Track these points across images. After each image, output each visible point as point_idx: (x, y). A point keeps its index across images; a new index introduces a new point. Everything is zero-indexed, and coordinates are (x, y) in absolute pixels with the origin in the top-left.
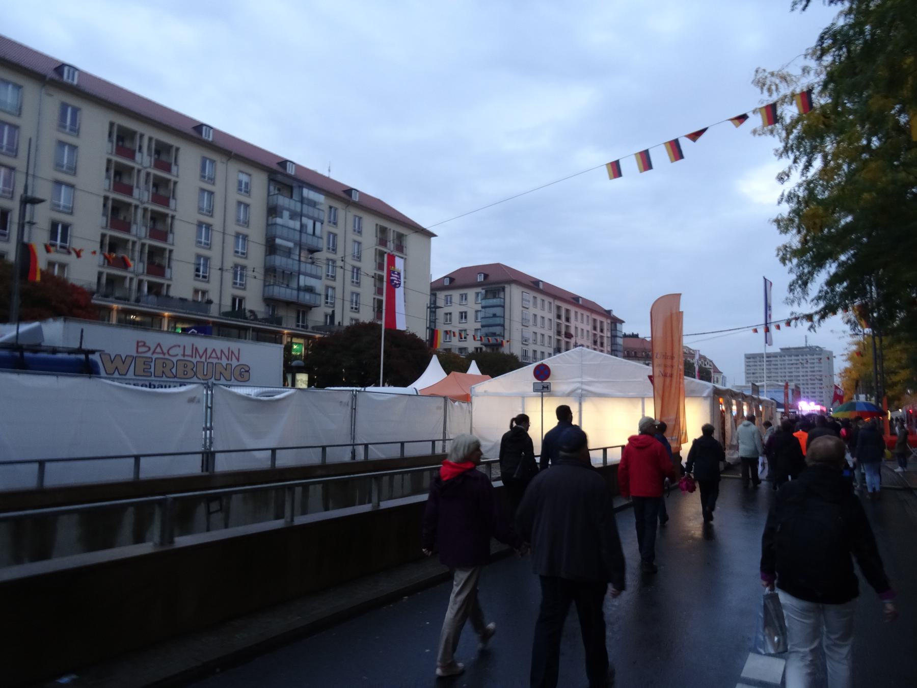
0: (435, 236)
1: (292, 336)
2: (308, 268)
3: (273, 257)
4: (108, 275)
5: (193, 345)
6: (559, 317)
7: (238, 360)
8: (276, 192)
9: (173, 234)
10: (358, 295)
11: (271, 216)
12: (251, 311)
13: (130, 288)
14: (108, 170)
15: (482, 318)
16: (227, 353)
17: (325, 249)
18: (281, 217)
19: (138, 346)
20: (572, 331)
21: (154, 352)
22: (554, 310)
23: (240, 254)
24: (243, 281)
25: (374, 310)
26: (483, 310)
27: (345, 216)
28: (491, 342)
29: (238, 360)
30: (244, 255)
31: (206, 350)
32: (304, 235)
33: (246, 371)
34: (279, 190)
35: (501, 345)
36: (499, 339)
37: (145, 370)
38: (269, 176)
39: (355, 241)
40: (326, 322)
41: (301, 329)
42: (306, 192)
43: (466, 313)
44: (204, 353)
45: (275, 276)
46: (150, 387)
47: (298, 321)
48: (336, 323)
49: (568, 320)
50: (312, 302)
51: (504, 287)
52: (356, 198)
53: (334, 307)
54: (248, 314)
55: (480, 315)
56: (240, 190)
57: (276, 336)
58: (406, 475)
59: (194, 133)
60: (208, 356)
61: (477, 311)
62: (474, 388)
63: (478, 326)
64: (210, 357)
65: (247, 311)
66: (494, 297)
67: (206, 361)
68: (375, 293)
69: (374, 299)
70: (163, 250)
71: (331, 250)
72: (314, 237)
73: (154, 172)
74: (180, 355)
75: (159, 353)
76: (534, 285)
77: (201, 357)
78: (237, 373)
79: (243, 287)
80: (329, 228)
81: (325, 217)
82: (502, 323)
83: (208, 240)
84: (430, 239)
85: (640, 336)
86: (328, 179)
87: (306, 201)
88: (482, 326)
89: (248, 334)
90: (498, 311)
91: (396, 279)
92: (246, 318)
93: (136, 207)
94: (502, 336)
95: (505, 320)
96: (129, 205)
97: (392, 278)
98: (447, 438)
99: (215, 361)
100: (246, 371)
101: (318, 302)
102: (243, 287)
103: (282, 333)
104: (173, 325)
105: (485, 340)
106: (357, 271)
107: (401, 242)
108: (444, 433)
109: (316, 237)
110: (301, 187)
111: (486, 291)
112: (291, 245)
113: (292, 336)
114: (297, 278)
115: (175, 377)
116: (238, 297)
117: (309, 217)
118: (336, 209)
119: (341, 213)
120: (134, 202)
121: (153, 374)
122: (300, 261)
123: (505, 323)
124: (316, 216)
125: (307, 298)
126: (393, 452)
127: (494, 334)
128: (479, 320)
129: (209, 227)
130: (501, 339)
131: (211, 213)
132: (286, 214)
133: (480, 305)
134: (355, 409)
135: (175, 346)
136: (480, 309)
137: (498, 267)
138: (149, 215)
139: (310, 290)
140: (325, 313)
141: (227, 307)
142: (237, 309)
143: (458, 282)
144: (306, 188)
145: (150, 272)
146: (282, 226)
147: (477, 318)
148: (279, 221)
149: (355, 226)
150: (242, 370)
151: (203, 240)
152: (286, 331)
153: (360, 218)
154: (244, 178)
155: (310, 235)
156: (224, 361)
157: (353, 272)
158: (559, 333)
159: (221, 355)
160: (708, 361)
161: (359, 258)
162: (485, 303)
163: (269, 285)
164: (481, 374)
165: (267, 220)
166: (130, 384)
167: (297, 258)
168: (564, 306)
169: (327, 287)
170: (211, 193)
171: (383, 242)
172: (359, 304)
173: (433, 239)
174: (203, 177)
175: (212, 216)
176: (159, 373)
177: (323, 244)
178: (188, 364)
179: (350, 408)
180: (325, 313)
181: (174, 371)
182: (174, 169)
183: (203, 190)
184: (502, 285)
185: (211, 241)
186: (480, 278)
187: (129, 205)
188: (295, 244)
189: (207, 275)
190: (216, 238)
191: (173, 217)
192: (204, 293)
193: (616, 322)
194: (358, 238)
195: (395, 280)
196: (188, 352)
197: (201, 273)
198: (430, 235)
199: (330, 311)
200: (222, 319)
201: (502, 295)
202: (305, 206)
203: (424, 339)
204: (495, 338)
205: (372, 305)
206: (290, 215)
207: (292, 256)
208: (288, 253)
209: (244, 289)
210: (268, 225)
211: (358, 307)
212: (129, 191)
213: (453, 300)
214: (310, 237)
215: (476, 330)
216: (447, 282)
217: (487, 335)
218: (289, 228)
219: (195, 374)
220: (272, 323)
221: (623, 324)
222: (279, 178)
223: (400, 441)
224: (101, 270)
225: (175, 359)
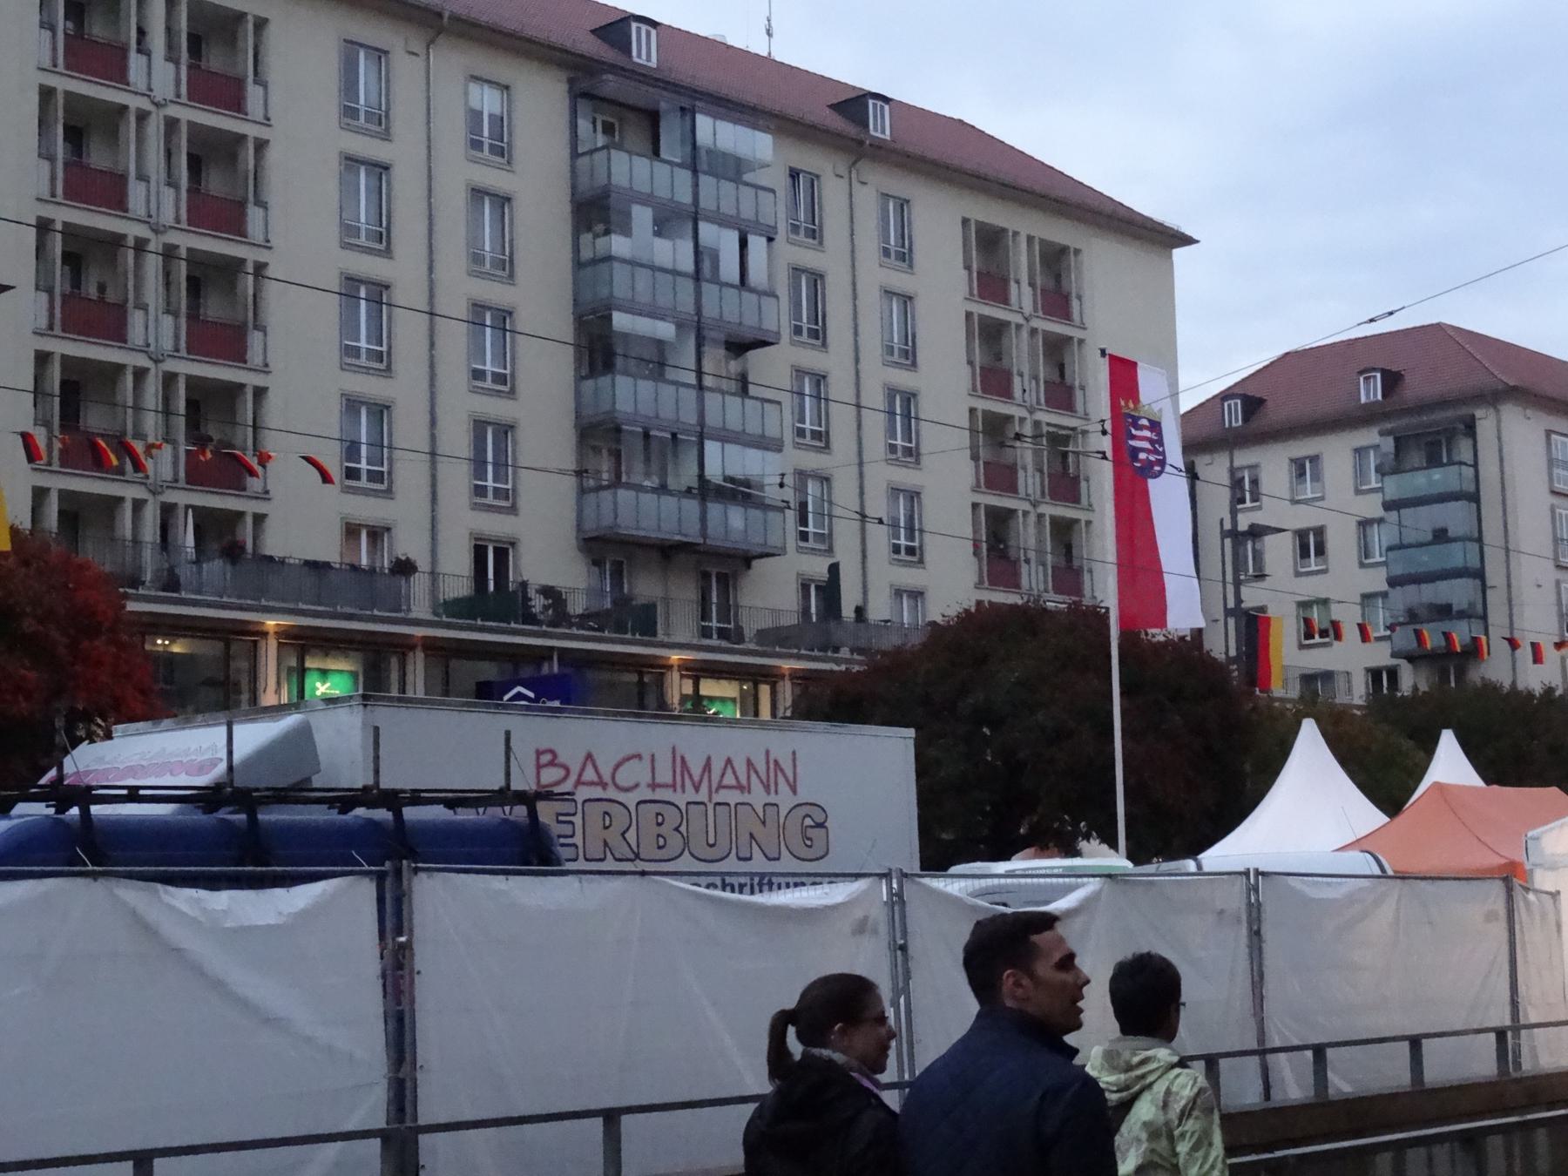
0: (1187, 241)
1: (698, 671)
2: (726, 410)
3: (604, 381)
4: (65, 495)
5: (767, 753)
7: (794, 791)
8: (601, 140)
9: (264, 330)
10: (913, 496)
11: (589, 229)
12: (547, 591)
13: (136, 542)
14: (44, 123)
15: (1390, 549)
16: (761, 768)
17: (786, 333)
18: (626, 231)
19: (539, 767)
21: (579, 782)
23: (488, 384)
24: (507, 483)
25: (976, 553)
26: (1393, 516)
28: (1429, 646)
29: (794, 791)
30: (505, 383)
31: (707, 766)
32: (709, 290)
33: (821, 825)
34: (608, 129)
35: (1474, 651)
36: (1461, 633)
37: (711, 841)
38: (571, 81)
39: (889, 293)
40: (806, 611)
41: (714, 642)
42: (713, 131)
43: (1320, 532)
44: (704, 771)
45: (617, 455)
46: (724, 890)
47: (705, 615)
48: (848, 612)
50: (755, 541)
51: (1473, 417)
52: (881, 127)
53: (830, 551)
54: (538, 603)
55: (1380, 538)
56: (476, 145)
57: (641, 674)
58: (1439, 1146)
59: (837, 122)
60: (714, 785)
61: (1364, 524)
62: (1537, 839)
63: (1376, 581)
64: (721, 787)
65: (532, 593)
66: (1434, 461)
67: (710, 801)
68: (978, 485)
69: (975, 506)
70: (233, 391)
71: (805, 337)
72: (745, 294)
73: (190, 115)
74: (643, 785)
75: (592, 783)
77: (697, 789)
78: (793, 829)
79: (383, 487)
80: (793, 253)
81: (776, 211)
82: (1474, 562)
83: (910, 442)
84: (1170, 257)
86: (767, 63)
87: (703, 164)
88: (1393, 582)
89: (410, 668)
90: (1455, 517)
91: (1146, 445)
92: (530, 618)
93: (140, 246)
94: (1477, 617)
95: (1486, 549)
96: (117, 240)
97: (1132, 443)
98: (1522, 1021)
99: (733, 797)
100: (821, 825)
101: (774, 540)
102: (508, 502)
103: (776, 676)
104: (293, 662)
105: (1405, 639)
106: (904, 405)
107: (1058, 278)
108: (1514, 1004)
109: (752, 290)
110: (688, 113)
111: (1397, 440)
112: (665, 330)
113: (698, 671)
114: (694, 452)
115: (637, 856)
116: (813, 581)
117: (723, 221)
118: (814, 179)
119: (833, 193)
120: (133, 230)
121: (581, 854)
122: (700, 387)
123: (1488, 568)
124: (747, 212)
125: (733, 523)
126: (1390, 1073)
127: (1444, 612)
128: (1378, 559)
129: (379, 292)
130: (1477, 630)
131: (383, 242)
132: (642, 217)
133: (1377, 499)
134: (903, 948)
135: (629, 759)
136: (1379, 512)
137: (1437, 335)
138: (57, 245)
139: (739, 492)
141: (458, 584)
142: (491, 587)
143: (1276, 413)
144: (708, 114)
145: (197, 476)
146: (633, 263)
147: (1366, 551)
148: (619, 245)
149: (886, 239)
150: (808, 822)
151: (363, 344)
152: (675, 657)
153: (903, 204)
154: (488, 101)
155: (732, 286)
156: (758, 797)
157: (892, 413)
159: (749, 778)
161: (909, 356)
162: (1395, 487)
163: (599, 488)
164: (1475, 780)
165: (576, 249)
166: (699, 886)
167: (691, 378)
169: (802, 476)
170: (381, 169)
171: (992, 285)
172: (921, 531)
173: (1179, 254)
174: (350, 112)
175: (387, 253)
176: (595, 849)
177: (777, 316)
178: (615, 809)
179: (884, 944)
181: (631, 836)
182: (253, 93)
183: (351, 162)
184: (1464, 411)
185: (390, 347)
186: (1371, 392)
187: (115, 241)
188: (680, 326)
190: (408, 332)
191: (260, 268)
192: (377, 534)
194: (899, 280)
195: (1143, 450)
196: (664, 776)
197: (363, 465)
198: (1169, 239)
199: (818, 568)
200: (448, 626)
201: (1464, 450)
202: (706, 181)
203: (1221, 657)
204: (1418, 627)
205: (969, 532)
206: (656, 222)
207: (670, 374)
208: (656, 361)
209: (513, 510)
210: (579, 264)
211: (916, 544)
212: (111, 193)
213: (1265, 486)
214: (731, 294)
215: (1367, 598)
216: (1234, 417)
217: (1413, 616)
218: (654, 268)
219: (686, 843)
220: (620, 628)
222: (611, 85)
223: (1408, 1033)
225: (630, 799)
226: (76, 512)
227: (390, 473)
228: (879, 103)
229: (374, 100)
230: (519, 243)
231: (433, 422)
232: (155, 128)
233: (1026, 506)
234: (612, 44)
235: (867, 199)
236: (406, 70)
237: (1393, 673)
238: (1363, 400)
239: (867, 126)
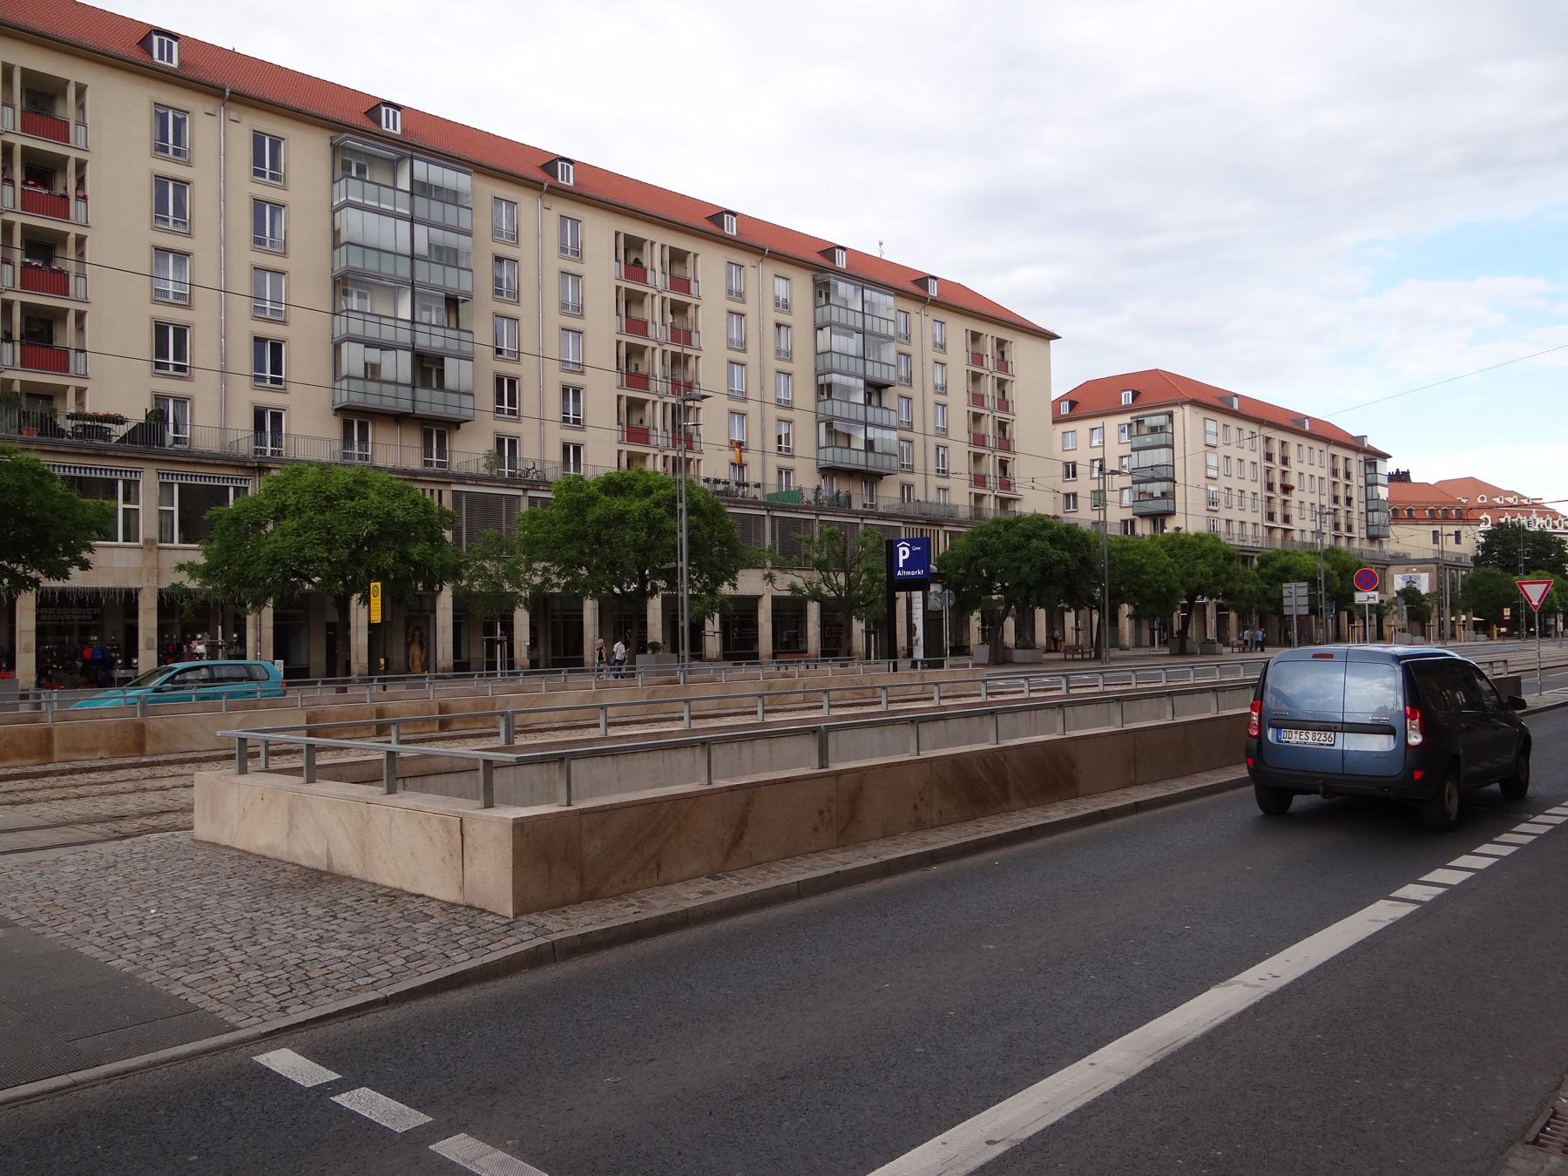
6: (1269, 457)
20: (1293, 480)
22: (1327, 463)
27: (924, 324)
49: (1285, 461)
50: (452, 413)
52: (731, 228)
59: (916, 290)
73: (670, 295)
76: (1217, 404)
82: (1170, 476)
85: (1414, 478)
90: (1161, 456)
119: (915, 319)
140: (936, 486)
158: (1270, 487)
160: (1560, 518)
168: (1278, 436)
171: (635, 269)
180: (936, 486)
189: (517, 409)
193: (1373, 457)
221: (1388, 460)
224: (621, 447)
226: (632, 458)
227: (519, 410)
228: (730, 216)
229: (510, 228)
230: (749, 332)
231: (925, 447)
232: (657, 300)
233: (990, 452)
234: (716, 224)
235: (551, 220)
236: (750, 272)
237: (1133, 522)
238: (1123, 403)
239: (723, 228)
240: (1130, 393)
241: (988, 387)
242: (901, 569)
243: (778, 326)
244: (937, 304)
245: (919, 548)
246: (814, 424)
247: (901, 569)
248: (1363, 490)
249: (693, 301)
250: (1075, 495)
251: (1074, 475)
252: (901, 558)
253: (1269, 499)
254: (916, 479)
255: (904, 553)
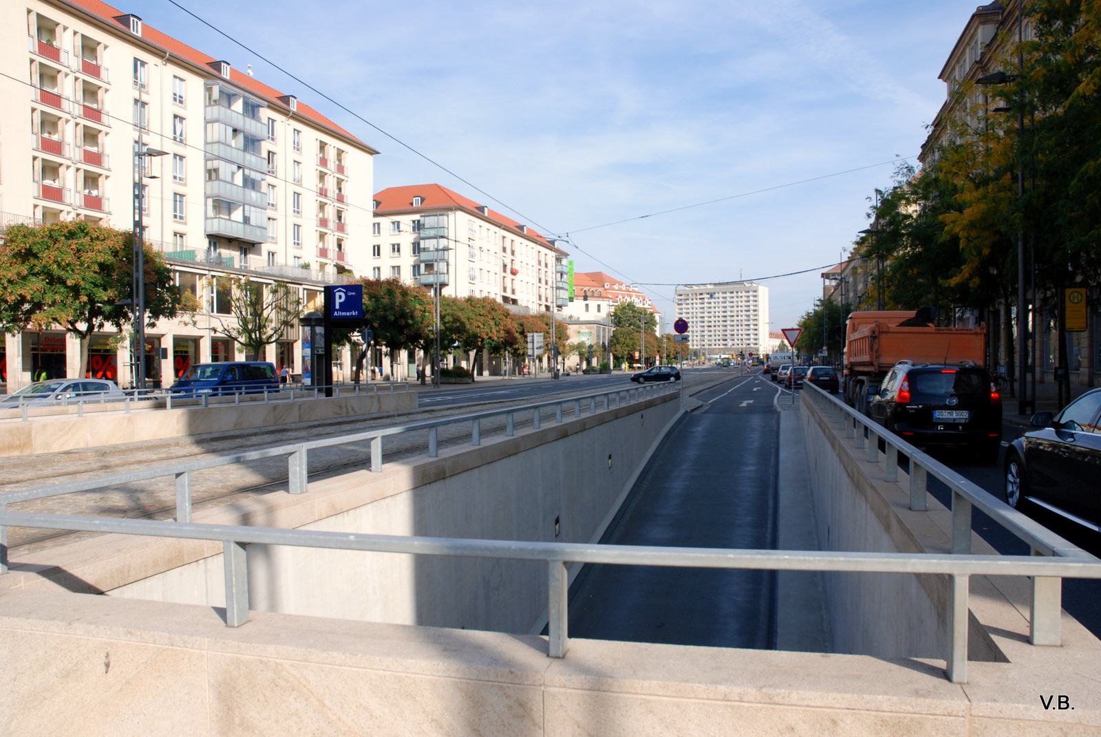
171: (48, 49)
240: (419, 198)
241: (331, 183)
242: (337, 310)
243: (175, 117)
244: (296, 117)
245: (354, 293)
246: (203, 200)
247: (337, 310)
248: (554, 275)
249: (104, 86)
250: (399, 267)
251: (379, 254)
252: (338, 301)
253: (504, 277)
254: (278, 248)
255: (340, 297)
